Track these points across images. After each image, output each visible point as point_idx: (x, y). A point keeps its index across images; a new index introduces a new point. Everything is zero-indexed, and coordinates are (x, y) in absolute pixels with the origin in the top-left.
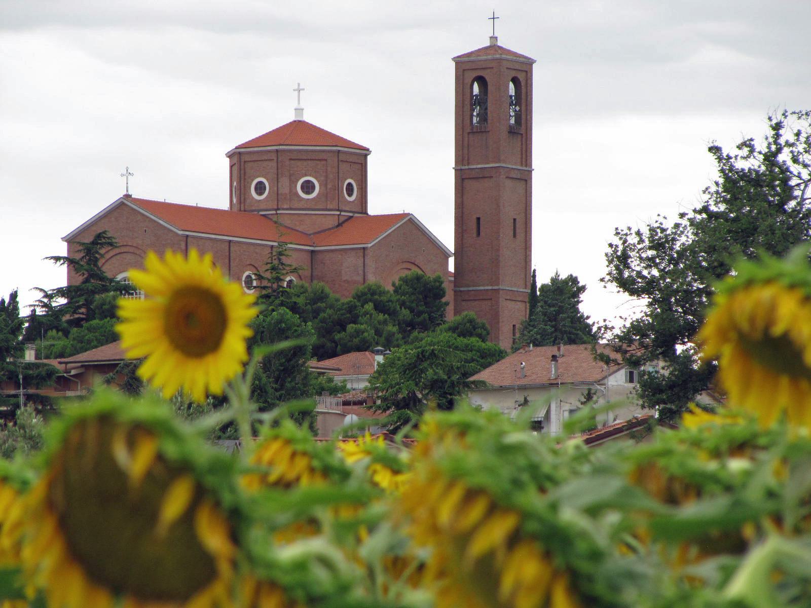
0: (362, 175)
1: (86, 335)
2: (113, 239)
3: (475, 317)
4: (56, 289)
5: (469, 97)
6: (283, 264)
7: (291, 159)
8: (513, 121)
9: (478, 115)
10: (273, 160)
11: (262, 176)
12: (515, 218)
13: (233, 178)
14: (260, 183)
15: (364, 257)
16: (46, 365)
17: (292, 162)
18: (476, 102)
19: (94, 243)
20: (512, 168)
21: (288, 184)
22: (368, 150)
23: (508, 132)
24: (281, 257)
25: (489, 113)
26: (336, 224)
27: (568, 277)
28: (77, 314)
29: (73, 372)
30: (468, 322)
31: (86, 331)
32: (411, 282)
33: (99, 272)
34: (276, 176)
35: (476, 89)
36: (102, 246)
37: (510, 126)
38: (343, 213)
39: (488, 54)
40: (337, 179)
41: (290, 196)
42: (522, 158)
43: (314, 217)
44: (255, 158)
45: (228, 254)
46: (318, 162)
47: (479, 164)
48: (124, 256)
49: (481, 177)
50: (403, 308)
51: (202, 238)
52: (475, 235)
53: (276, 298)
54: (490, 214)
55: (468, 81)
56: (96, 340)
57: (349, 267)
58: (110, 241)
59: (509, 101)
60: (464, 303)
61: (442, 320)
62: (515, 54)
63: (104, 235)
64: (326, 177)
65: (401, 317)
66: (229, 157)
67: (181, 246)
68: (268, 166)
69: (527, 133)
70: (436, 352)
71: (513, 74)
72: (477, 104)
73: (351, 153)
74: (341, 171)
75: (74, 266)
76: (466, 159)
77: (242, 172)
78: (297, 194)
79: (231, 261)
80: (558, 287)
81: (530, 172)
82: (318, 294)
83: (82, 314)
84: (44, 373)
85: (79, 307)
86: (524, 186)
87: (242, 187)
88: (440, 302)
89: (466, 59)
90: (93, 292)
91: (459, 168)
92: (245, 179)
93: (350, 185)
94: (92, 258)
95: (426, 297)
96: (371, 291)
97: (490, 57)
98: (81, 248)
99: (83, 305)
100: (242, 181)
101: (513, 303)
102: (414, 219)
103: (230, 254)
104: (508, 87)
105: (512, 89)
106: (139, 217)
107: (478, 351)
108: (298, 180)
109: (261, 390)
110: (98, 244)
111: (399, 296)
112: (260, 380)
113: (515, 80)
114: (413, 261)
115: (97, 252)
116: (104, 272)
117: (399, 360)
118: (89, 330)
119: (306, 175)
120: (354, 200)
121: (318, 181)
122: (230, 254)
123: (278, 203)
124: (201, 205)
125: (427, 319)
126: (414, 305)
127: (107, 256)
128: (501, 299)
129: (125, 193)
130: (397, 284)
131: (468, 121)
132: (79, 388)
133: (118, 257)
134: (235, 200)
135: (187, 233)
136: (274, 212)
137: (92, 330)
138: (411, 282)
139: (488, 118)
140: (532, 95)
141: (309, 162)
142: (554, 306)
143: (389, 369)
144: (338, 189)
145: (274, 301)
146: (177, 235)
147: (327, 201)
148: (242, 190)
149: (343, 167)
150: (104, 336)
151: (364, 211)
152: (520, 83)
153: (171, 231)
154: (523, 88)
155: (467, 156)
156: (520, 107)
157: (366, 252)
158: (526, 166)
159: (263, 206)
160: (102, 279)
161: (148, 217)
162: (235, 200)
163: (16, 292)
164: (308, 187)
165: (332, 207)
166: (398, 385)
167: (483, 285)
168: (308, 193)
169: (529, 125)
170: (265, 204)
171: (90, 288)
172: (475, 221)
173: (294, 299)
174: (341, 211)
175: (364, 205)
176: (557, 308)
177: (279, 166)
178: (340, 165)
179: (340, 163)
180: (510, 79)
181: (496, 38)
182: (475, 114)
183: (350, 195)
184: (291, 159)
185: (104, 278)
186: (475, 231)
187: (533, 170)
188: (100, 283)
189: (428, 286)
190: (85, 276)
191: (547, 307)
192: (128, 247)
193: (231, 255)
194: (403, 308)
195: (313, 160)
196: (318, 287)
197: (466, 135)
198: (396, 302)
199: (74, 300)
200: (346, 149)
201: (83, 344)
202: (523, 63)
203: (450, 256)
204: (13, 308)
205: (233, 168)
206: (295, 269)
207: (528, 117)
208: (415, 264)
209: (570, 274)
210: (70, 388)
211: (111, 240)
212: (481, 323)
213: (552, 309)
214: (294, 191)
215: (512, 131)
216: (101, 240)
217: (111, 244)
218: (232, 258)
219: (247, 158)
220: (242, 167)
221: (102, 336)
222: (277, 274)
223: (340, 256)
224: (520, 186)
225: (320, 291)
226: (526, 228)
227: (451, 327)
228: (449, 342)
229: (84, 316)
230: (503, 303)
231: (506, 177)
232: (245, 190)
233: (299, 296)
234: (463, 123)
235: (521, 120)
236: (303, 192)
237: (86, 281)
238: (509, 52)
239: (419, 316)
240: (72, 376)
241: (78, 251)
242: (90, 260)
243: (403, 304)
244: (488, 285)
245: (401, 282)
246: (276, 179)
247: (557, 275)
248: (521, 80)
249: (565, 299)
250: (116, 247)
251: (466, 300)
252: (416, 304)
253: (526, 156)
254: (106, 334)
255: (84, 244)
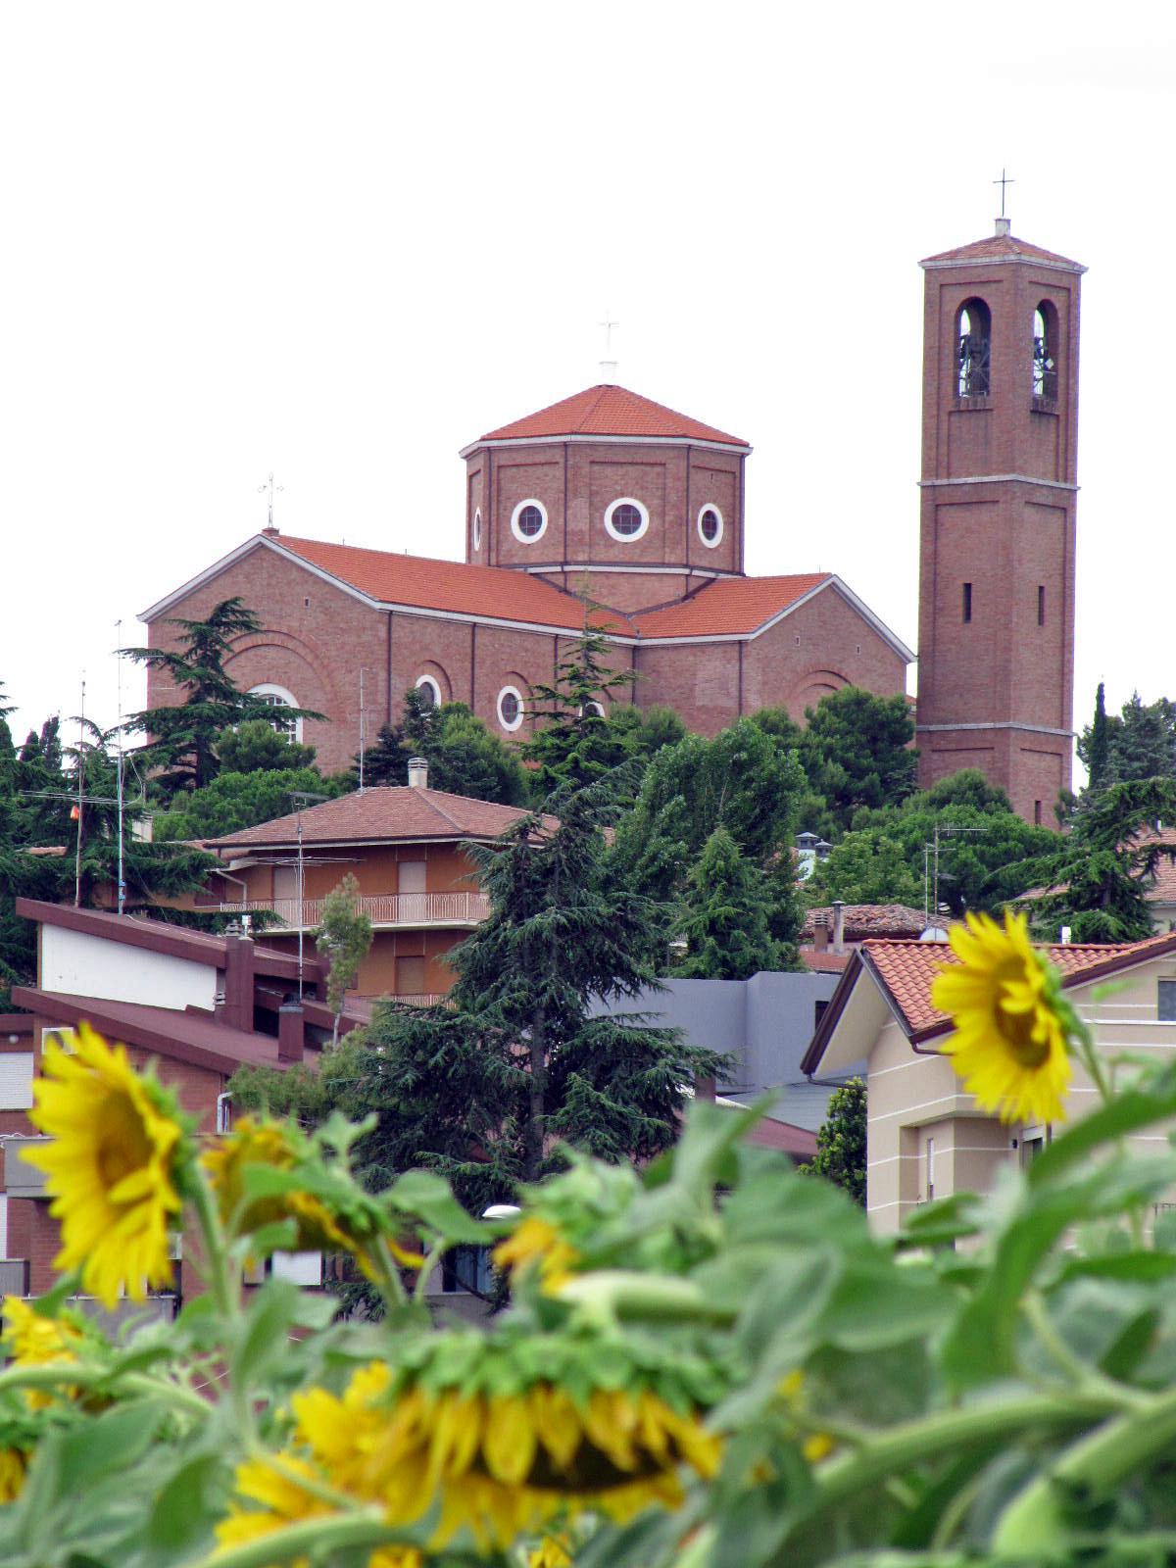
0: (734, 496)
1: (217, 803)
2: (251, 615)
3: (984, 778)
4: (138, 715)
5: (951, 341)
6: (594, 668)
7: (592, 462)
8: (1039, 389)
9: (969, 375)
10: (557, 463)
11: (536, 496)
12: (1042, 585)
13: (473, 499)
14: (531, 509)
15: (740, 660)
16: (183, 848)
17: (596, 468)
18: (967, 352)
19: (214, 622)
20: (1038, 485)
21: (586, 511)
22: (746, 445)
23: (1032, 412)
24: (591, 654)
25: (992, 373)
26: (682, 593)
27: (1158, 704)
28: (177, 764)
29: (234, 866)
30: (970, 789)
31: (216, 795)
32: (845, 710)
33: (223, 682)
34: (562, 495)
35: (966, 325)
36: (229, 630)
37: (1035, 400)
38: (696, 573)
39: (992, 254)
40: (685, 503)
41: (590, 535)
42: (1057, 464)
43: (638, 580)
44: (520, 458)
45: (469, 650)
46: (648, 468)
47: (970, 475)
48: (262, 651)
49: (975, 503)
50: (830, 760)
51: (419, 618)
52: (960, 619)
53: (580, 737)
54: (992, 576)
55: (951, 307)
56: (238, 811)
57: (711, 678)
58: (245, 618)
59: (1032, 348)
60: (935, 756)
61: (910, 786)
62: (1046, 254)
63: (233, 606)
64: (664, 498)
65: (826, 779)
66: (466, 457)
67: (380, 634)
68: (546, 475)
69: (1067, 415)
70: (1160, 790)
71: (1042, 294)
72: (967, 355)
73: (712, 452)
74: (692, 488)
75: (173, 670)
76: (945, 464)
77: (494, 487)
78: (604, 532)
79: (477, 665)
80: (1149, 720)
81: (1073, 492)
82: (662, 729)
83: (189, 764)
84: (185, 864)
85: (183, 751)
86: (1060, 522)
87: (494, 518)
88: (903, 750)
89: (948, 263)
90: (211, 721)
91: (929, 483)
92: (498, 502)
93: (709, 514)
94: (208, 653)
95: (874, 740)
96: (768, 725)
97: (996, 259)
98: (186, 632)
99: (191, 746)
100: (494, 506)
101: (1036, 756)
102: (840, 585)
103: (473, 651)
104: (1032, 320)
105: (1039, 324)
106: (294, 575)
107: (1019, 841)
108: (606, 505)
109: (729, 880)
110: (219, 624)
111: (821, 737)
112: (727, 859)
113: (1046, 308)
114: (836, 671)
115: (218, 641)
116: (233, 682)
117: (860, 857)
118: (222, 790)
119: (622, 495)
120: (719, 546)
121: (648, 507)
122: (473, 651)
123: (565, 549)
124: (411, 553)
125: (878, 782)
126: (851, 755)
127: (237, 647)
128: (1012, 749)
129: (266, 526)
130: (815, 713)
131: (950, 389)
132: (245, 898)
133: (251, 653)
134: (477, 545)
135: (391, 607)
136: (559, 569)
137: (228, 792)
138: (845, 710)
139: (990, 383)
140: (1078, 337)
141: (630, 468)
142: (1138, 758)
143: (841, 875)
144: (687, 523)
145: (577, 742)
146: (372, 610)
147: (664, 547)
148: (494, 524)
149: (699, 479)
150: (253, 804)
151: (737, 569)
152: (1055, 311)
153: (359, 602)
154: (1062, 322)
155: (946, 459)
156: (1056, 361)
157: (744, 650)
158: (1066, 480)
159: (534, 558)
160: (228, 694)
161: (312, 574)
162: (477, 545)
163: (56, 720)
164: (627, 519)
165: (673, 559)
166: (1079, 857)
167: (975, 721)
168: (626, 530)
169: (1072, 396)
170: (538, 552)
171: (206, 711)
172: (961, 590)
173: (616, 739)
174: (692, 568)
175: (737, 556)
176: (1146, 764)
177: (569, 476)
178: (690, 476)
179: (692, 470)
180: (1036, 304)
181: (1008, 221)
182: (963, 374)
183: (710, 535)
184: (592, 462)
185: (232, 694)
186: (961, 610)
187: (1079, 488)
188: (224, 702)
189: (880, 717)
190: (195, 689)
191: (1125, 761)
192: (271, 635)
193: (476, 652)
194: (830, 760)
195: (637, 464)
196: (661, 715)
197: (944, 417)
198: (818, 747)
199: (174, 736)
200: (704, 444)
201: (211, 820)
202: (1063, 272)
203: (910, 661)
204: (49, 751)
205: (474, 480)
206: (620, 678)
207: (1071, 381)
208: (841, 677)
209: (1161, 698)
210: (225, 898)
211: (247, 616)
212: (996, 792)
213: (1136, 764)
214: (598, 526)
215: (1039, 411)
216: (226, 616)
217: (247, 625)
218: (477, 660)
219: (503, 459)
220: (494, 478)
221: (248, 805)
222: (583, 688)
223: (691, 658)
224: (1055, 520)
225: (666, 724)
226: (1064, 605)
227: (935, 799)
228: (961, 822)
229: (193, 770)
230: (1016, 757)
231: (1027, 503)
232: (498, 524)
233: (623, 733)
234: (938, 393)
235: (1056, 386)
236: (617, 529)
237: (196, 699)
238: (1033, 250)
239: (861, 778)
240: (231, 873)
241: (181, 638)
242: (204, 656)
243: (829, 752)
244: (985, 721)
245: (825, 710)
246: (562, 502)
247: (1136, 700)
248: (1057, 306)
249: (1160, 745)
250: (257, 631)
251: (940, 751)
252: (856, 754)
253: (1066, 460)
254: (256, 801)
255: (192, 624)
